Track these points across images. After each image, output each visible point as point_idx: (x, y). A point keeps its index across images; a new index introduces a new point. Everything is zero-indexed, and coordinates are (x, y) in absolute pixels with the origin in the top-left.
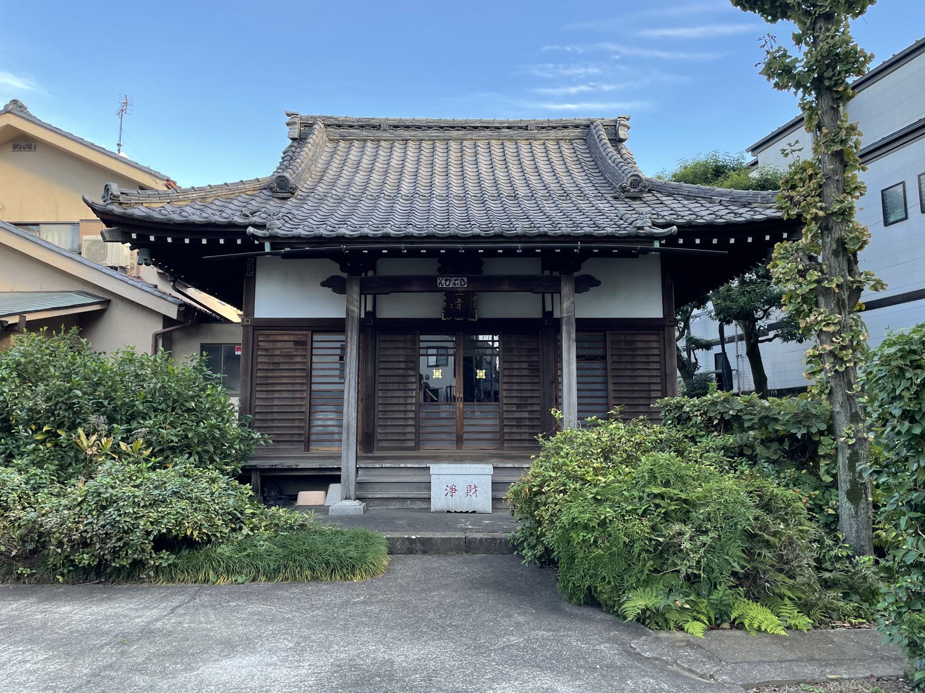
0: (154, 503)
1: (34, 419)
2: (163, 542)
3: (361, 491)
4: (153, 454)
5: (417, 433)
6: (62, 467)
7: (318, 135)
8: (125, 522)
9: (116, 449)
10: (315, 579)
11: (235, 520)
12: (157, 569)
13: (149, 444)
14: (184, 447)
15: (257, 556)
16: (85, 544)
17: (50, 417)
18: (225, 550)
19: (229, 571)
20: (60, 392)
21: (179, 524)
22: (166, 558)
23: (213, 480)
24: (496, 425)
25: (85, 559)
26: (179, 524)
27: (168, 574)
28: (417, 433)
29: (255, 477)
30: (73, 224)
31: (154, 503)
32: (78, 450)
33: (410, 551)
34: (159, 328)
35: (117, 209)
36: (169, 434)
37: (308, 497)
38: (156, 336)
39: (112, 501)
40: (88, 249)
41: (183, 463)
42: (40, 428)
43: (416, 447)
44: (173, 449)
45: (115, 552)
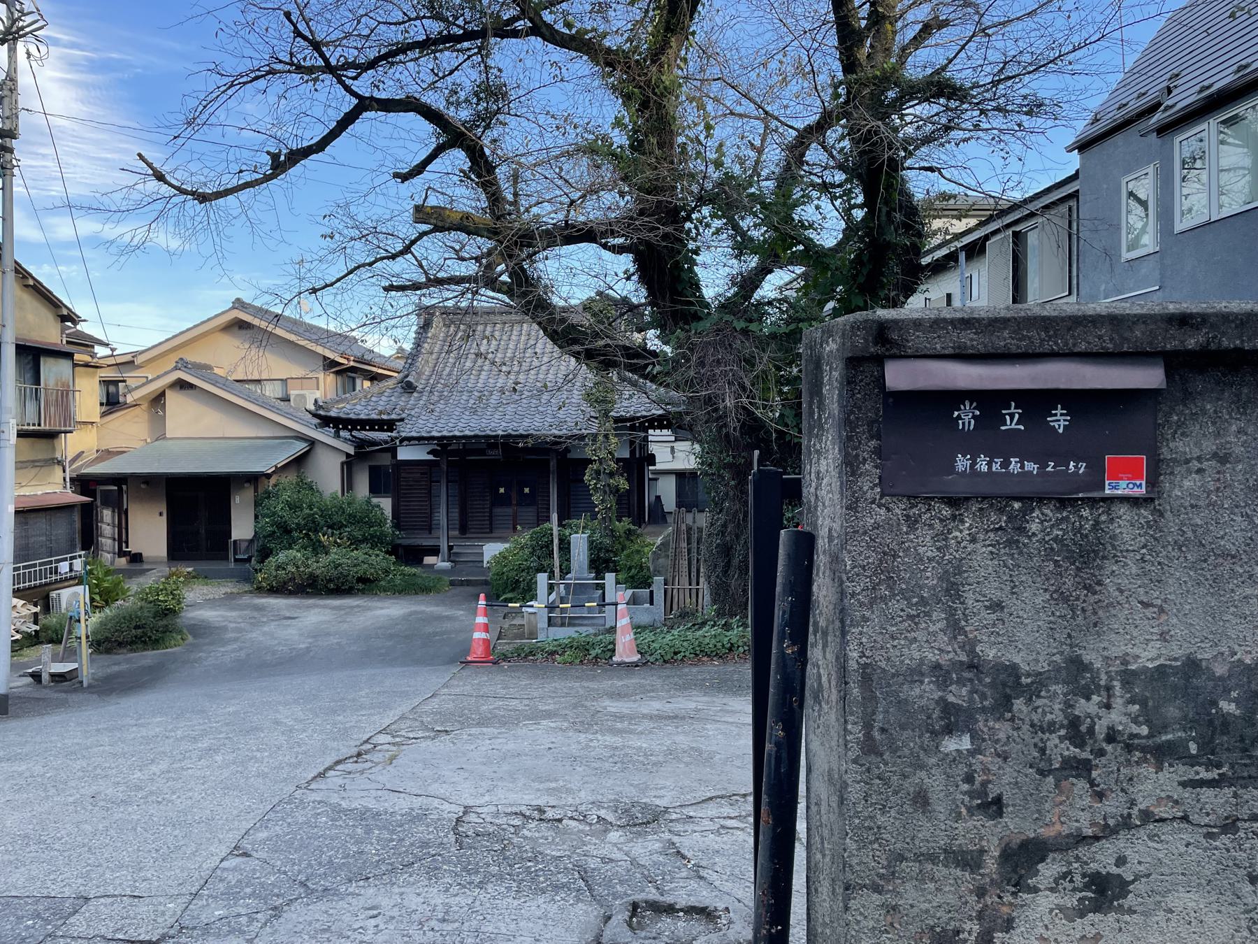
0: (355, 566)
1: (299, 528)
2: (360, 580)
3: (452, 556)
4: (351, 544)
5: (491, 524)
6: (314, 549)
7: (437, 321)
8: (345, 573)
9: (336, 542)
10: (416, 594)
11: (387, 572)
12: (358, 590)
13: (349, 539)
14: (365, 540)
15: (395, 585)
16: (330, 580)
17: (848, 857)
18: (383, 583)
19: (385, 591)
20: (309, 515)
21: (365, 573)
22: (361, 586)
23: (377, 555)
24: (192, 606)
25: (332, 586)
26: (365, 573)
27: (363, 592)
28: (491, 524)
29: (401, 551)
30: (282, 380)
31: (355, 566)
32: (320, 542)
33: (462, 585)
34: (344, 459)
35: (322, 413)
36: (358, 534)
37: (429, 560)
38: (342, 464)
39: (340, 565)
40: (295, 400)
41: (365, 547)
42: (301, 532)
43: (491, 532)
44: (360, 541)
45: (343, 583)
